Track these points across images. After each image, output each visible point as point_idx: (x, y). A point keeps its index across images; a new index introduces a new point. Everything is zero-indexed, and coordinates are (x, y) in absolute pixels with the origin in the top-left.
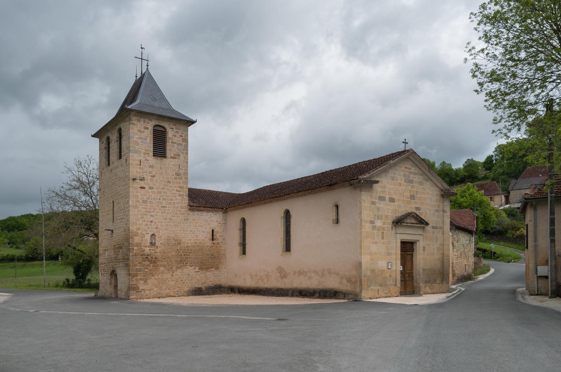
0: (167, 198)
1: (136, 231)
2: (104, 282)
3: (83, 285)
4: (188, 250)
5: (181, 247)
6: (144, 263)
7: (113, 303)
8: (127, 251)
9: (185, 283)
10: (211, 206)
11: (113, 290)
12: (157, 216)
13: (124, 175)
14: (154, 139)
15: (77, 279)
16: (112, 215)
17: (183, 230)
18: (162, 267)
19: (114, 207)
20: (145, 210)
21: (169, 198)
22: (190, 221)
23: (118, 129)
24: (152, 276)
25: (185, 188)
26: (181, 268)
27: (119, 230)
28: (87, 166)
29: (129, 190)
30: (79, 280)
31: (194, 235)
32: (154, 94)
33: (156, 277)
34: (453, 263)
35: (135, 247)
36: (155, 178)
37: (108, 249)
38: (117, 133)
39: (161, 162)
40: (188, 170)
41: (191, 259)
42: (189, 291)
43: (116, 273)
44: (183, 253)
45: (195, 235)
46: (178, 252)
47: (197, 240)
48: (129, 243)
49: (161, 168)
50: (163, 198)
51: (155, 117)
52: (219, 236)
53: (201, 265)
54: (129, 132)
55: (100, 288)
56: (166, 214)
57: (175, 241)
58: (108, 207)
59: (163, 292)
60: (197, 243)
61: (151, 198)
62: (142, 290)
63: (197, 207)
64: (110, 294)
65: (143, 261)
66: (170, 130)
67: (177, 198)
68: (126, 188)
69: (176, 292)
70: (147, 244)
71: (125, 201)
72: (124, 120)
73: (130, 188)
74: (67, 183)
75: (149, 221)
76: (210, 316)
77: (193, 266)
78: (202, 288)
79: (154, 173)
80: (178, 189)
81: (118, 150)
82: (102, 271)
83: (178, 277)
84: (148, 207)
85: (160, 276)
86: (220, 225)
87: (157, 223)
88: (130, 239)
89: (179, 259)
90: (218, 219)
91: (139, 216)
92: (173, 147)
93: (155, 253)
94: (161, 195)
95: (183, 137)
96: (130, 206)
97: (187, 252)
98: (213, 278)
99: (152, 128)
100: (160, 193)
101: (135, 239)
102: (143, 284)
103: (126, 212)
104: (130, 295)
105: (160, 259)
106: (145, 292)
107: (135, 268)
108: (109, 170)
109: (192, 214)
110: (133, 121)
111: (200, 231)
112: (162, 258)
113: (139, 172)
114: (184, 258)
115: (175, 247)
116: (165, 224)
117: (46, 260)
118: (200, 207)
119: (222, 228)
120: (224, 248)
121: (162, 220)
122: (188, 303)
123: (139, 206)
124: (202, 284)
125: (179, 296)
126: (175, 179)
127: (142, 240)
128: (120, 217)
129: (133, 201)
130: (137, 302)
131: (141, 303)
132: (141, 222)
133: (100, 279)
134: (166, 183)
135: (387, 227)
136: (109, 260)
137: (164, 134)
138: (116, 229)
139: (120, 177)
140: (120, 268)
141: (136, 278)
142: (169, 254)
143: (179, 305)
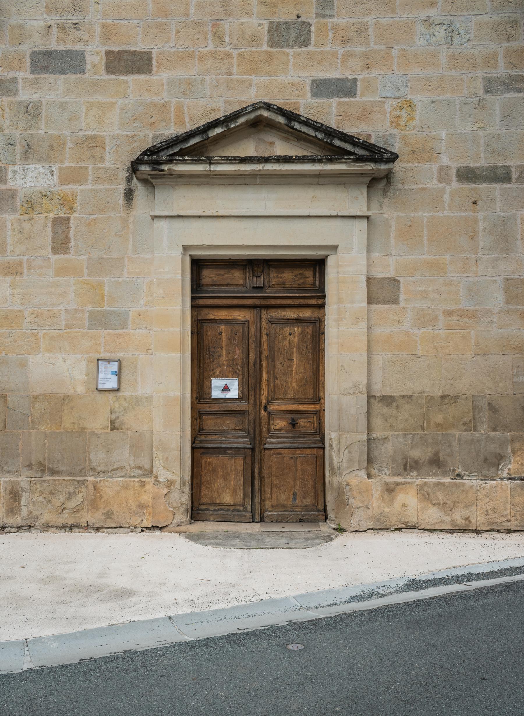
34: (295, 479)
135: (91, 190)
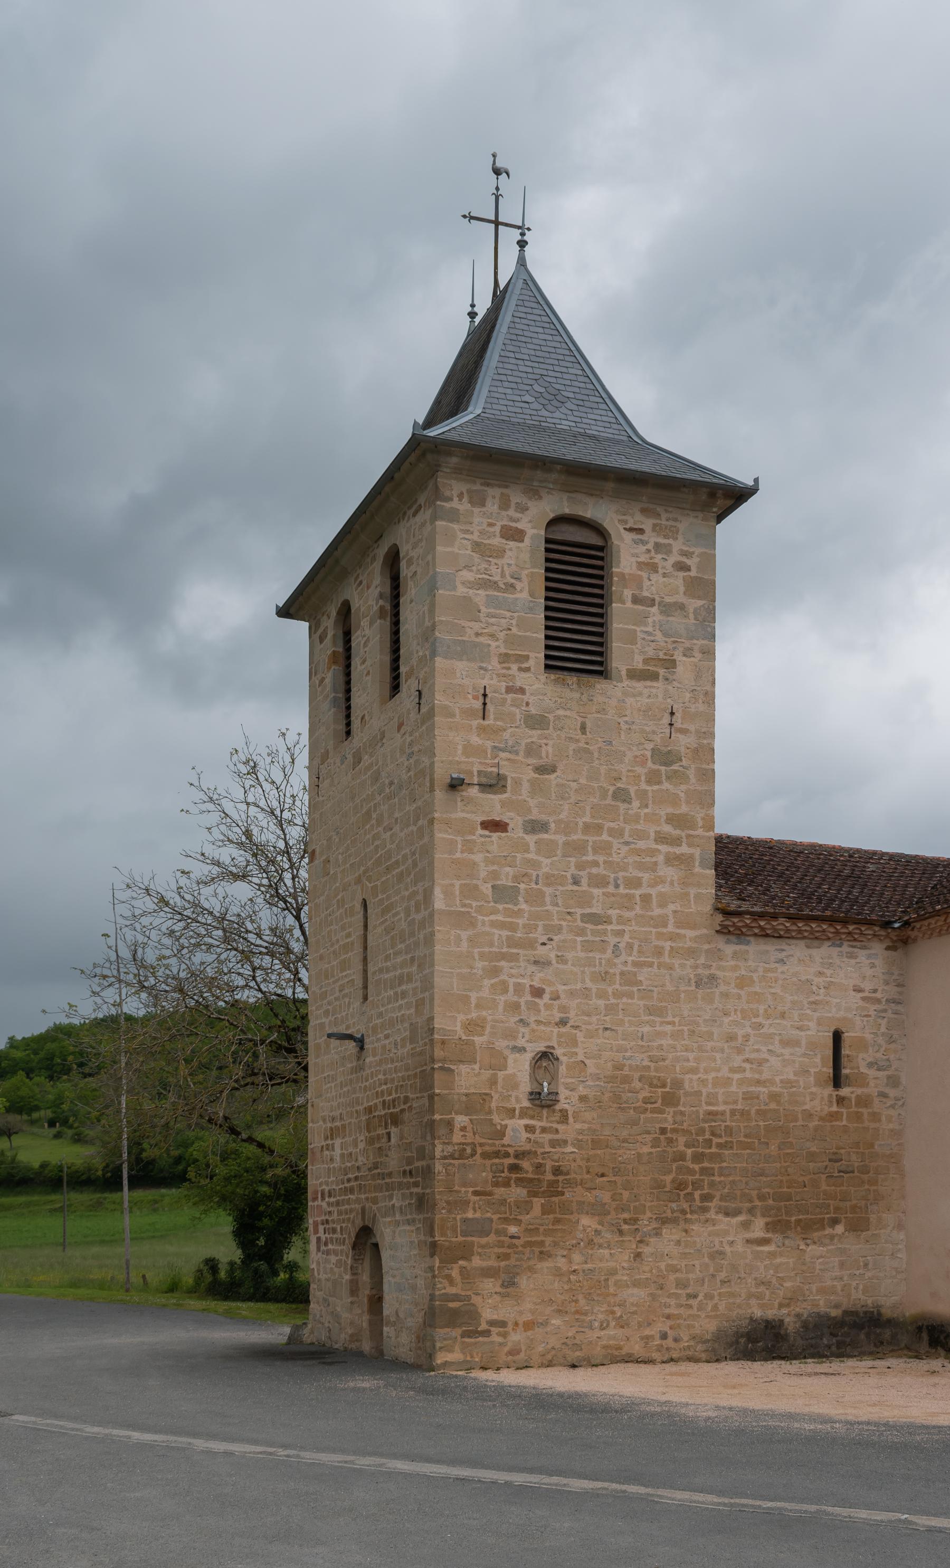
0: (612, 876)
1: (464, 1038)
2: (327, 1280)
3: (268, 1289)
4: (713, 1134)
5: (679, 1118)
6: (500, 1192)
7: (352, 1384)
8: (423, 1137)
9: (700, 1297)
10: (828, 913)
11: (366, 1317)
12: (565, 962)
13: (409, 770)
14: (547, 589)
15: (248, 1259)
16: (361, 967)
17: (692, 1033)
18: (587, 1213)
19: (370, 927)
20: (505, 933)
21: (621, 874)
22: (723, 988)
23: (387, 556)
24: (541, 1259)
25: (700, 823)
26: (682, 1223)
27: (387, 1037)
28: (278, 776)
29: (432, 836)
30: (255, 1265)
31: (741, 1058)
32: (551, 373)
33: (561, 1262)
35: (457, 1113)
36: (553, 776)
37: (344, 1126)
38: (382, 573)
39: (585, 697)
40: (712, 735)
41: (731, 1178)
42: (718, 1336)
43: (378, 1239)
44: (687, 1145)
45: (747, 1060)
46: (664, 1143)
47: (759, 1082)
48: (431, 1097)
49: (583, 728)
50: (590, 876)
51: (554, 476)
52: (870, 1065)
53: (779, 1209)
54: (434, 558)
55: (312, 1305)
56: (610, 951)
57: (651, 1085)
58: (344, 933)
59: (593, 1335)
60: (758, 1098)
61: (535, 874)
62: (492, 1323)
63: (762, 915)
64: (352, 1336)
65: (496, 1184)
66: (629, 537)
67: (661, 873)
68: (421, 829)
69: (657, 1342)
70: (518, 1100)
71: (415, 893)
72: (409, 508)
73: (436, 826)
74: (203, 854)
75: (528, 989)
76: (863, 1514)
77: (737, 1213)
78: (782, 1321)
79: (548, 753)
80: (667, 829)
81: (387, 658)
82: (321, 1228)
83: (663, 1265)
84: (521, 922)
85: (577, 1257)
86: (872, 1008)
87: (562, 996)
88: (437, 1076)
89: (668, 1178)
90: (864, 977)
91: (480, 964)
92: (642, 619)
93: (554, 1143)
94: (584, 858)
95: (688, 569)
96: (436, 917)
97: (708, 1143)
98: (837, 1273)
99: (543, 533)
100: (578, 848)
101: (460, 1074)
102: (497, 1298)
103: (417, 944)
104: (434, 1346)
105: (579, 1177)
106: (505, 1335)
107: (459, 1217)
108: (350, 757)
109: (735, 955)
110: (450, 499)
111: (771, 1036)
112: (588, 1172)
113: (479, 751)
114: (691, 1172)
115: (649, 1115)
116: (601, 1003)
117: (132, 1187)
118: (775, 917)
119: (884, 1022)
120: (891, 1126)
121: (589, 984)
122: (717, 1407)
123: (480, 918)
124: (781, 1306)
125: (672, 1360)
126: (649, 782)
127: (493, 1082)
128: (392, 974)
129: (448, 893)
130: (465, 1388)
131: (482, 1393)
132: (486, 993)
133: (314, 1266)
134: (609, 801)
136: (349, 1180)
137: (599, 563)
138: (375, 1030)
139: (391, 783)
140: (394, 1214)
141: (462, 1268)
142: (620, 1152)
143: (670, 1416)
